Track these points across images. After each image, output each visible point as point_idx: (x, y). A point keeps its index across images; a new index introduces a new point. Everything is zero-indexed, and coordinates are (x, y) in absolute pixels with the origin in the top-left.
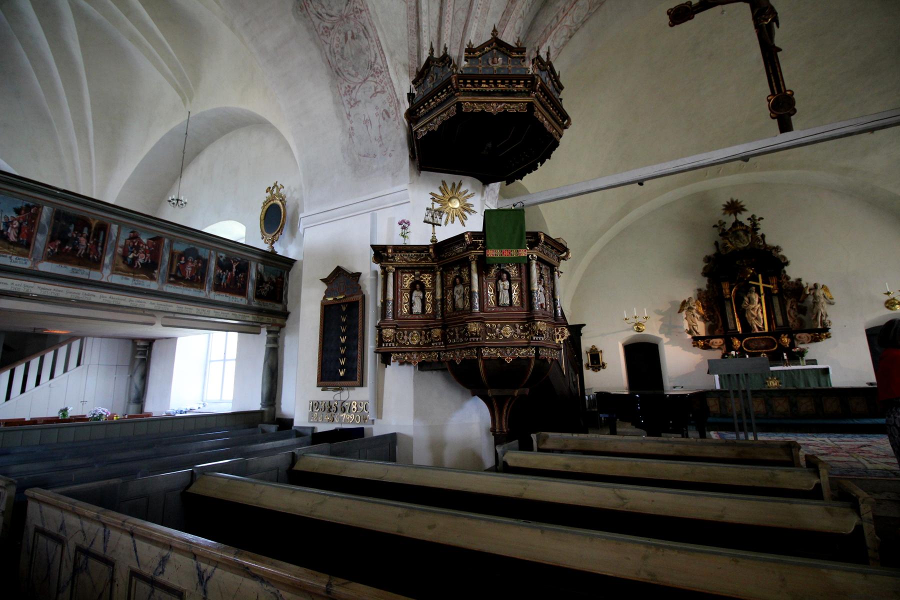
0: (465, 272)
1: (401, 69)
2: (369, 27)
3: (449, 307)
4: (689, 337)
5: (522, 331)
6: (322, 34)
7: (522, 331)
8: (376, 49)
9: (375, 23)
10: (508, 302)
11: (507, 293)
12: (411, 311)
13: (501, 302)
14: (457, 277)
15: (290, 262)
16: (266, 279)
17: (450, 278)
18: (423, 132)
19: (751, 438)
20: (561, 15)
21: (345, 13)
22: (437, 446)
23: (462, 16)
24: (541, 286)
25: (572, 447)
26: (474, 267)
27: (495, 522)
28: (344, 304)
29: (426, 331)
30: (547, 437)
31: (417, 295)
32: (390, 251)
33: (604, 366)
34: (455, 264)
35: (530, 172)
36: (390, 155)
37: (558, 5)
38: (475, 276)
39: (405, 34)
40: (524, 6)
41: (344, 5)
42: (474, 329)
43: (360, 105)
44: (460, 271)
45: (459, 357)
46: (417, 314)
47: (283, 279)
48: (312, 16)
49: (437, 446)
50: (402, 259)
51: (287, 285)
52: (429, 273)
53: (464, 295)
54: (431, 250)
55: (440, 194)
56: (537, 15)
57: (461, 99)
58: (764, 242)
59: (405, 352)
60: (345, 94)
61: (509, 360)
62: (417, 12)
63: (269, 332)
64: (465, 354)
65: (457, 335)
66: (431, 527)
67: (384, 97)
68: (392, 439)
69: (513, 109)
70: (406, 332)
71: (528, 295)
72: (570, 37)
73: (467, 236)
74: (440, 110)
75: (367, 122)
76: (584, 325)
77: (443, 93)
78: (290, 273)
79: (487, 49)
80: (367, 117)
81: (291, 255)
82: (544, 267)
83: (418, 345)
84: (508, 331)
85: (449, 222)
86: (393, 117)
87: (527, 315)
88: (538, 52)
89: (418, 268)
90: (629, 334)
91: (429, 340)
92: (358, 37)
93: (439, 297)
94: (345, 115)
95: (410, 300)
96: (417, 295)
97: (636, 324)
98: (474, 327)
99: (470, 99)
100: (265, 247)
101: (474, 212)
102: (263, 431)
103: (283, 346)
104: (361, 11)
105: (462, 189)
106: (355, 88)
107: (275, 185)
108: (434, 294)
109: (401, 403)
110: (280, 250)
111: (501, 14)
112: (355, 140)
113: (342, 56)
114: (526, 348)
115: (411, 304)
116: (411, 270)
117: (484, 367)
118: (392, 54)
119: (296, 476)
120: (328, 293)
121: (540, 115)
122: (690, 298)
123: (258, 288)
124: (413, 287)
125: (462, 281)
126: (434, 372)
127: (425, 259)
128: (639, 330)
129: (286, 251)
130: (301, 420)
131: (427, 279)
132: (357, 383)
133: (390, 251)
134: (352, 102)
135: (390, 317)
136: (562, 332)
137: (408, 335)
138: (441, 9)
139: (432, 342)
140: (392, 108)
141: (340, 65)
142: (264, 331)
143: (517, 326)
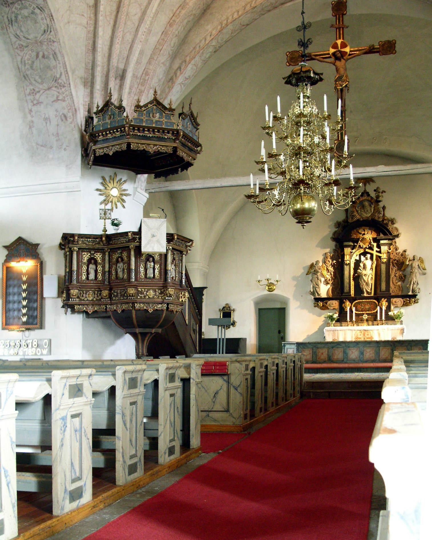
1: (78, 81)
2: (58, 52)
3: (113, 277)
5: (160, 294)
6: (17, 48)
7: (160, 294)
8: (62, 69)
9: (64, 52)
10: (152, 276)
11: (152, 271)
12: (87, 278)
13: (148, 276)
14: (119, 257)
17: (115, 256)
21: (39, 39)
24: (173, 265)
26: (132, 253)
29: (98, 291)
31: (92, 267)
34: (119, 248)
35: (173, 174)
36: (65, 149)
38: (133, 259)
41: (40, 35)
42: (132, 292)
43: (42, 106)
44: (121, 253)
46: (92, 280)
50: (83, 243)
52: (101, 252)
53: (123, 270)
54: (104, 239)
56: (190, 31)
57: (130, 140)
58: (384, 215)
59: (84, 305)
60: (29, 94)
61: (151, 311)
64: (124, 307)
65: (119, 295)
67: (64, 104)
69: (164, 149)
70: (84, 292)
71: (165, 272)
73: (130, 234)
75: (47, 120)
76: (206, 288)
77: (117, 131)
79: (150, 106)
80: (47, 116)
82: (175, 253)
83: (92, 300)
84: (151, 293)
86: (70, 120)
87: (163, 284)
89: (94, 249)
91: (100, 297)
92: (48, 57)
93: (107, 269)
94: (27, 110)
95: (87, 270)
96: (92, 267)
99: (137, 141)
104: (54, 42)
106: (39, 92)
108: (104, 267)
111: (160, 33)
113: (32, 67)
114: (161, 304)
115: (88, 274)
116: (89, 250)
117: (135, 315)
118: (73, 72)
122: (317, 262)
124: (89, 261)
125: (122, 260)
126: (96, 319)
127: (99, 243)
128: (270, 290)
131: (98, 256)
133: (76, 238)
134: (35, 102)
135: (75, 282)
136: (184, 295)
137: (86, 294)
139: (102, 298)
140: (70, 114)
141: (28, 73)
143: (157, 290)
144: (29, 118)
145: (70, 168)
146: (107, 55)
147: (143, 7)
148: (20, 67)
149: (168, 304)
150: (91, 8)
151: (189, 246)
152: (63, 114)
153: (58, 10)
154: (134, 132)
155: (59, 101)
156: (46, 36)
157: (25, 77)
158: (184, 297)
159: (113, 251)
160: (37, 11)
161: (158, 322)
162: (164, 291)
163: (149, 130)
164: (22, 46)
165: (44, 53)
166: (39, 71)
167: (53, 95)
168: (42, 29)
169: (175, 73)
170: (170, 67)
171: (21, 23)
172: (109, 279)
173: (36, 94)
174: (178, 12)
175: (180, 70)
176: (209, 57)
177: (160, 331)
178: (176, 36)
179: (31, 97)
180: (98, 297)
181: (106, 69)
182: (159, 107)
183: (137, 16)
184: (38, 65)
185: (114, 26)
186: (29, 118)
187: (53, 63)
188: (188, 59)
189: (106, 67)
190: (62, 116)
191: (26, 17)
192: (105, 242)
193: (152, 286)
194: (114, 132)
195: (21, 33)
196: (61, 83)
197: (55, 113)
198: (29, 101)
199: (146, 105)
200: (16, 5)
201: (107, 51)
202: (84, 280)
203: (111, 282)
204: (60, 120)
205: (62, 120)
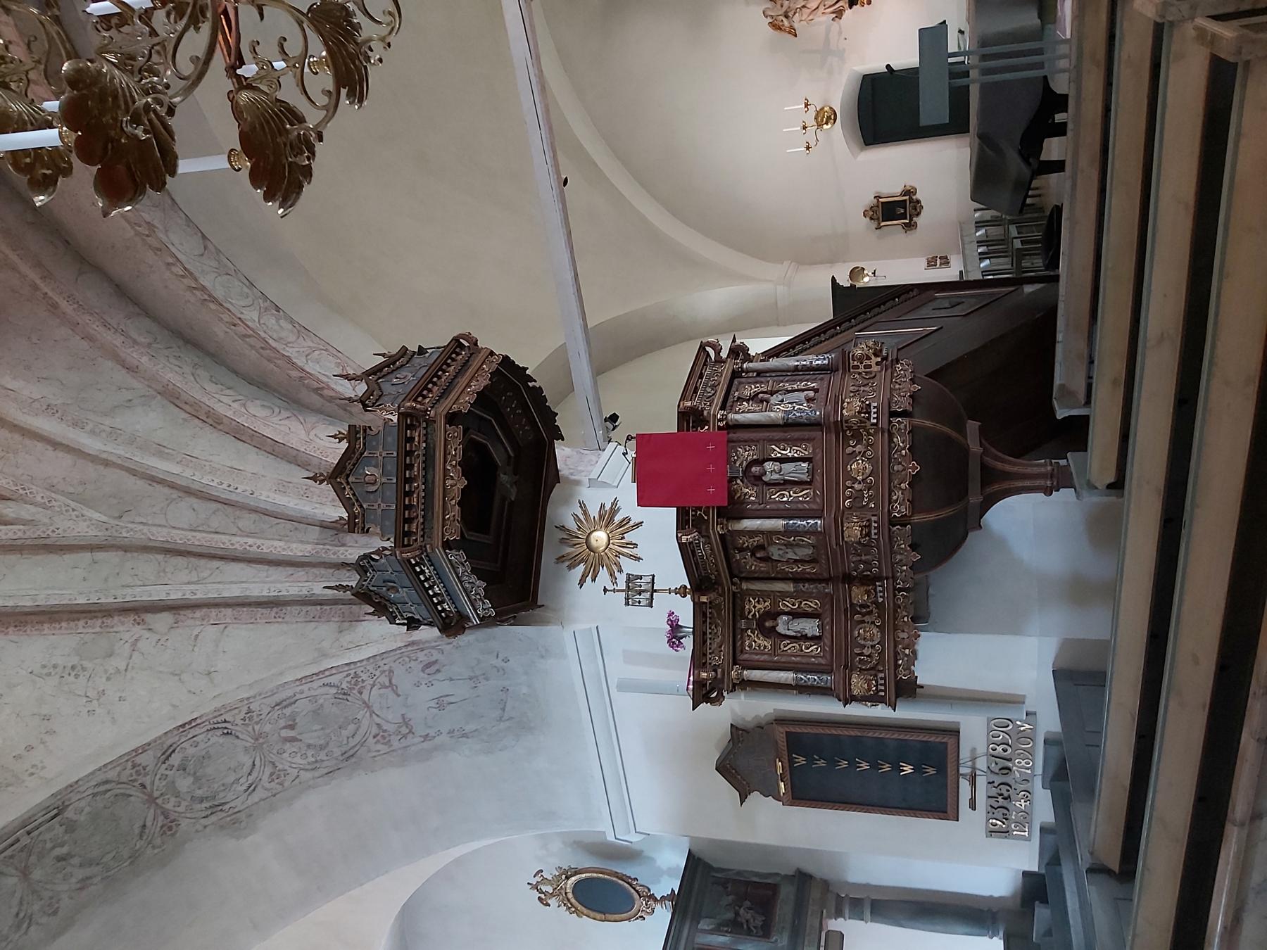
0: (744, 541)
1: (347, 638)
2: (277, 698)
4: (848, 13)
8: (315, 685)
10: (805, 465)
12: (816, 639)
13: (805, 477)
14: (753, 555)
15: (694, 862)
16: (730, 915)
18: (485, 608)
19: (1063, 64)
20: (241, 329)
22: (1079, 591)
23: (247, 521)
25: (1082, 345)
27: (1184, 569)
28: (791, 761)
30: (1062, 386)
32: (704, 675)
33: (909, 192)
37: (221, 335)
39: (285, 627)
40: (224, 399)
41: (237, 741)
42: (857, 531)
43: (409, 715)
44: (741, 550)
45: (906, 556)
46: (821, 627)
47: (727, 881)
48: (249, 802)
49: (1079, 591)
51: (739, 873)
53: (788, 545)
54: (704, 599)
55: (582, 567)
56: (236, 373)
60: (388, 743)
61: (914, 468)
62: (243, 605)
63: (839, 914)
66: (1196, 661)
67: (399, 671)
68: (1063, 676)
69: (456, 450)
70: (857, 651)
71: (790, 428)
72: (278, 309)
74: (452, 577)
75: (441, 703)
77: (422, 572)
78: (715, 865)
80: (433, 704)
81: (679, 861)
84: (858, 467)
85: (634, 552)
88: (350, 399)
90: (837, 134)
91: (873, 607)
92: (293, 717)
93: (790, 587)
94: (426, 745)
97: (820, 125)
98: (853, 531)
100: (662, 917)
101: (615, 503)
102: (1049, 933)
103: (867, 887)
105: (571, 525)
107: (535, 887)
108: (784, 595)
109: (994, 659)
110: (669, 884)
112: (468, 728)
113: (322, 748)
114: (891, 435)
116: (736, 635)
117: (928, 511)
118: (325, 655)
119: (1125, 870)
120: (770, 791)
121: (464, 400)
123: (749, 932)
124: (770, 633)
125: (761, 547)
128: (832, 118)
129: (670, 872)
130: (1023, 856)
131: (755, 607)
132: (950, 741)
133: (704, 675)
134: (404, 730)
138: (235, 559)
140: (421, 656)
142: (834, 924)
143: (850, 450)
144: (444, 738)
145: (547, 650)
146: (290, 570)
147: (175, 494)
148: (326, 771)
149: (893, 414)
150: (181, 617)
151: (718, 353)
152: (423, 671)
153: (174, 706)
154: (416, 534)
155: (394, 681)
156: (238, 730)
157: (348, 756)
158: (869, 358)
159: (735, 572)
160: (176, 759)
161: (948, 438)
162: (850, 428)
163: (409, 494)
164: (272, 774)
165: (285, 727)
166: (328, 731)
167: (381, 695)
168: (221, 740)
169: (331, 399)
170: (319, 411)
171: (216, 786)
172: (820, 581)
173: (385, 731)
174: (187, 408)
175: (322, 389)
176: (292, 322)
177: (973, 426)
178: (244, 405)
179: (395, 739)
180: (870, 613)
181: (323, 571)
182: (349, 467)
183: (195, 506)
184: (316, 734)
185: (222, 558)
186: (444, 738)
187: (303, 706)
188: (294, 374)
189: (315, 570)
190: (427, 671)
191: (197, 779)
192: (713, 595)
193: (837, 463)
194: (427, 580)
195: (242, 781)
196: (349, 682)
197: (423, 687)
198: (404, 743)
199: (347, 503)
200: (169, 806)
201: (280, 568)
202: (823, 650)
203: (826, 575)
204: (439, 676)
205: (438, 671)
